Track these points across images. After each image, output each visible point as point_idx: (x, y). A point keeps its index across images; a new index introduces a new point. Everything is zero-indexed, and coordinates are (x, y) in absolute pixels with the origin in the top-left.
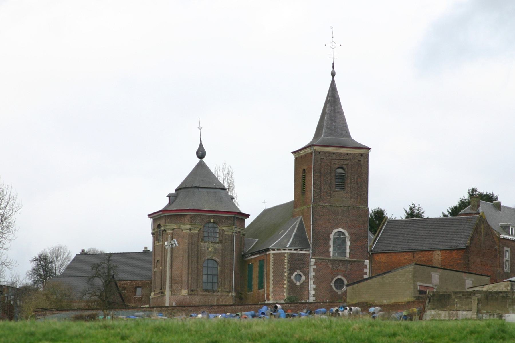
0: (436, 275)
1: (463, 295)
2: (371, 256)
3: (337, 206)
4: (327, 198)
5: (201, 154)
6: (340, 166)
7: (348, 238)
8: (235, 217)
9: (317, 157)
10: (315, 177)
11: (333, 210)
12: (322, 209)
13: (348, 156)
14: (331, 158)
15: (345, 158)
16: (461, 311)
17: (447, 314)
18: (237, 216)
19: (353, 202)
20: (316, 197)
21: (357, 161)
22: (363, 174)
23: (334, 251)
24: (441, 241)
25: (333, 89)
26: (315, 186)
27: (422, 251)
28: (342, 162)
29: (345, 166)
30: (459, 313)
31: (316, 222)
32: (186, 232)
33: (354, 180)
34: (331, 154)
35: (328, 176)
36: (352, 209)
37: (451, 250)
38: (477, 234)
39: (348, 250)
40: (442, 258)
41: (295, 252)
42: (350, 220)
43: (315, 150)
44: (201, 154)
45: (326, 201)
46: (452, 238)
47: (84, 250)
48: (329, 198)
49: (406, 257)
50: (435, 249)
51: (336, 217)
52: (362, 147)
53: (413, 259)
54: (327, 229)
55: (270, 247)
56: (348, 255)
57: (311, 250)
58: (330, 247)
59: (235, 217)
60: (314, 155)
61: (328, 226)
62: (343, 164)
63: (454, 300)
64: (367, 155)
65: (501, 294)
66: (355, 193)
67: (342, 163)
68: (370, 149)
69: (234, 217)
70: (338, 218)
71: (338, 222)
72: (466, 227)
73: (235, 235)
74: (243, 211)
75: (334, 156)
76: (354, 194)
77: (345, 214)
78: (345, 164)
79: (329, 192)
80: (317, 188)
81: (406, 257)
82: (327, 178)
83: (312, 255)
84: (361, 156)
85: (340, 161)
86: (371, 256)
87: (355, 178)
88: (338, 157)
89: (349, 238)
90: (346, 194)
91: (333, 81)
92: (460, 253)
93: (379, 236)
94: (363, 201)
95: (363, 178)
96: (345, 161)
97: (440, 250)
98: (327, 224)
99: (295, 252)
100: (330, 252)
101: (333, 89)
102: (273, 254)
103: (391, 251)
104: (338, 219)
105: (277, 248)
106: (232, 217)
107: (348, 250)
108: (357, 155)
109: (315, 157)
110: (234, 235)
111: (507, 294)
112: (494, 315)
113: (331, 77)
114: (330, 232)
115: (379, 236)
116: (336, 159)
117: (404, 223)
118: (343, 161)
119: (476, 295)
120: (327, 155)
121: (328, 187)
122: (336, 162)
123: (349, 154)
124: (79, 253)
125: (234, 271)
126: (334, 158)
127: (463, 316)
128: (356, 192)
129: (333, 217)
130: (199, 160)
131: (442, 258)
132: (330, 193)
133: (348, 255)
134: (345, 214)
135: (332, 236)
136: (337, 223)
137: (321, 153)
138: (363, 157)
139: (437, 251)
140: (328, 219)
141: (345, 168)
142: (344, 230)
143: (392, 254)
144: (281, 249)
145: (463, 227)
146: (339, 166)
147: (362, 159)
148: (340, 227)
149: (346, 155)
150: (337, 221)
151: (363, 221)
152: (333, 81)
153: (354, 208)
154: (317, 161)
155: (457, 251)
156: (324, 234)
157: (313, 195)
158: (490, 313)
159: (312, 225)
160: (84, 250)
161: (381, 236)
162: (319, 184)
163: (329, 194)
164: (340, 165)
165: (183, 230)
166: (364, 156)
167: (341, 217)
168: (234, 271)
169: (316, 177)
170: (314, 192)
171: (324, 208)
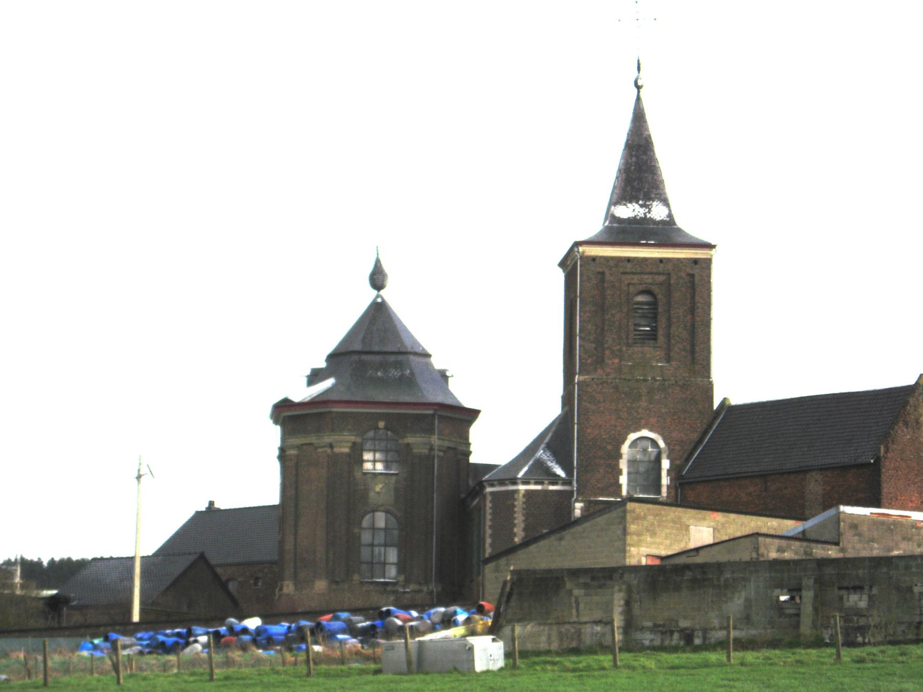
0: (705, 529)
1: (593, 579)
2: (679, 490)
3: (638, 381)
4: (613, 363)
5: (377, 279)
6: (645, 289)
7: (665, 452)
8: (436, 417)
9: (587, 270)
10: (582, 315)
11: (628, 389)
12: (600, 387)
13: (662, 265)
14: (621, 270)
15: (655, 270)
16: (588, 625)
17: (554, 634)
18: (439, 413)
19: (676, 369)
20: (587, 360)
21: (684, 275)
22: (699, 305)
23: (631, 484)
24: (767, 447)
25: (639, 117)
26: (583, 335)
27: (782, 474)
28: (648, 279)
29: (656, 289)
30: (583, 631)
31: (586, 417)
32: (322, 452)
33: (701, 323)
34: (622, 261)
35: (614, 312)
36: (673, 384)
37: (845, 468)
38: (907, 428)
39: (665, 480)
40: (824, 489)
41: (539, 487)
42: (668, 410)
43: (583, 252)
44: (377, 279)
45: (611, 369)
46: (851, 440)
47: (213, 502)
48: (616, 361)
49: (751, 489)
50: (809, 468)
51: (634, 405)
52: (695, 242)
53: (764, 494)
54: (613, 432)
55: (484, 479)
56: (664, 490)
57: (575, 483)
58: (668, 471)
59: (436, 417)
60: (581, 266)
61: (616, 426)
62: (651, 284)
63: (570, 592)
64: (708, 262)
65: (690, 573)
66: (679, 349)
67: (650, 281)
68: (713, 247)
69: (433, 416)
70: (638, 408)
71: (639, 416)
72: (885, 412)
73: (436, 456)
74: (467, 403)
75: (629, 265)
76: (678, 350)
77: (657, 397)
78: (656, 284)
79: (618, 347)
80: (589, 340)
81: (751, 489)
82: (613, 315)
83: (578, 494)
84: (693, 265)
85: (643, 276)
86: (679, 490)
87: (681, 313)
88: (639, 269)
89: (667, 453)
90: (658, 353)
91: (638, 99)
92: (863, 476)
93: (704, 443)
94: (700, 366)
95: (699, 314)
96: (657, 277)
97: (821, 469)
98: (613, 422)
99: (539, 487)
100: (620, 486)
101: (639, 117)
102: (492, 493)
103: (719, 477)
104: (640, 410)
105: (535, 479)
106: (427, 415)
107: (665, 480)
108: (684, 261)
109: (583, 268)
110: (434, 456)
111: (704, 573)
112: (672, 632)
113: (636, 90)
114: (621, 441)
115: (704, 443)
116: (634, 271)
117: (759, 409)
118: (651, 276)
119: (626, 577)
120: (612, 265)
121: (615, 337)
122: (636, 279)
123: (664, 261)
124: (204, 509)
125: (434, 537)
126: (628, 270)
127: (594, 638)
128: (682, 348)
129: (628, 404)
130: (375, 292)
131: (824, 489)
132: (620, 351)
133: (664, 490)
134: (657, 397)
135: (625, 449)
136: (637, 419)
137: (597, 261)
138: (697, 266)
139: (814, 473)
140: (616, 410)
141: (656, 292)
142: (655, 433)
143: (722, 483)
144: (507, 482)
145: (877, 413)
146: (641, 288)
147: (696, 271)
148: (644, 428)
149: (659, 262)
150: (638, 413)
151: (700, 412)
152: (638, 99)
153: (676, 382)
154: (589, 279)
155: (856, 470)
156: (605, 445)
157: (580, 356)
158: (661, 629)
159: (578, 424)
160: (213, 502)
161: (707, 442)
162: (593, 331)
163: (618, 353)
164: (645, 285)
165: (316, 448)
166: (700, 264)
167: (645, 404)
168: (434, 537)
169: (585, 316)
170: (582, 348)
171: (605, 385)
